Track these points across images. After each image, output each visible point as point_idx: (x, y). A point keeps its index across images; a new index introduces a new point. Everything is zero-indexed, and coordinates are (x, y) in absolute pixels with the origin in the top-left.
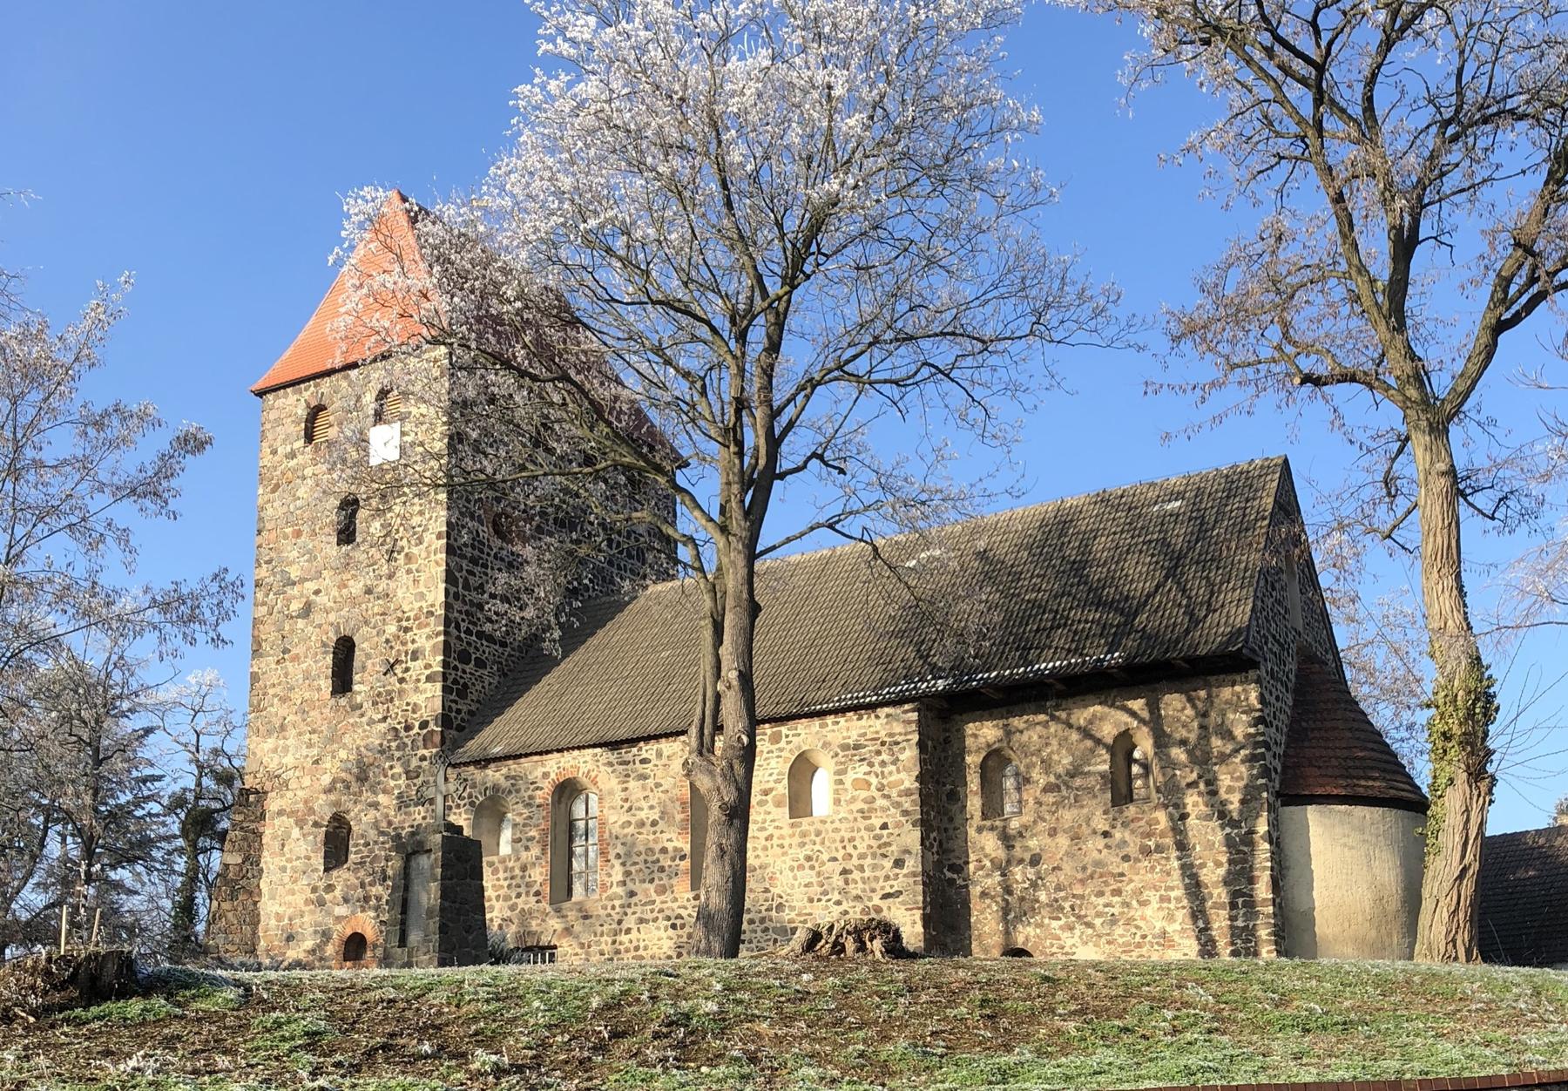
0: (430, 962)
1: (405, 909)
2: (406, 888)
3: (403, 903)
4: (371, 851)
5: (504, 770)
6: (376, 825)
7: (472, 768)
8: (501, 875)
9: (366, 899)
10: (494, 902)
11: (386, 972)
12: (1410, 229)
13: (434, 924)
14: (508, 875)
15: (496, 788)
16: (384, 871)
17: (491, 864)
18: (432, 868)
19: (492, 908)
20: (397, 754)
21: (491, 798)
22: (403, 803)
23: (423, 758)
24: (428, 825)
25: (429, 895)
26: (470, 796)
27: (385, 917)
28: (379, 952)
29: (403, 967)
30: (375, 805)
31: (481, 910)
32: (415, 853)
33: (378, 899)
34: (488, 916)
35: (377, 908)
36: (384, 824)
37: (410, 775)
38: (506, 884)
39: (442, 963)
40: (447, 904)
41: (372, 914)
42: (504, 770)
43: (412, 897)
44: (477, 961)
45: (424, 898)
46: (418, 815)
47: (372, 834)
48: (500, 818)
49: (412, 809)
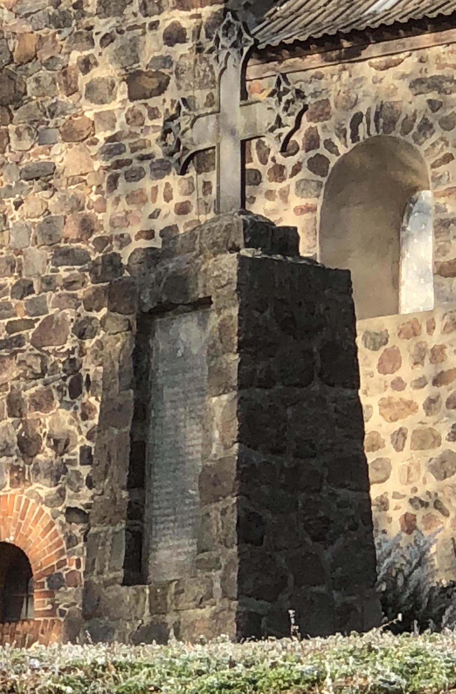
0: (214, 632)
1: (138, 474)
2: (142, 413)
3: (134, 454)
4: (37, 308)
5: (409, 64)
6: (48, 232)
7: (314, 60)
8: (407, 371)
9: (27, 446)
10: (388, 451)
11: (94, 653)
12: (369, 14)
13: (224, 514)
14: (427, 370)
15: (385, 116)
16: (73, 366)
17: (378, 341)
18: (213, 353)
19: (385, 468)
20: (103, 26)
21: (372, 147)
22: (123, 165)
23: (174, 36)
24: (197, 229)
25: (207, 428)
26: (312, 141)
27: (83, 497)
28: (70, 598)
29: (141, 637)
30: (44, 176)
31: (356, 472)
32: (163, 309)
33: (61, 445)
34: (375, 492)
35: (58, 473)
36: (71, 230)
37: (141, 84)
38: (420, 397)
39: (251, 628)
40: (258, 458)
41: (44, 489)
42: (409, 64)
43: (158, 438)
44: (347, 621)
45: (193, 438)
46: (167, 201)
47: (38, 257)
48: (400, 201)
49: (147, 184)
